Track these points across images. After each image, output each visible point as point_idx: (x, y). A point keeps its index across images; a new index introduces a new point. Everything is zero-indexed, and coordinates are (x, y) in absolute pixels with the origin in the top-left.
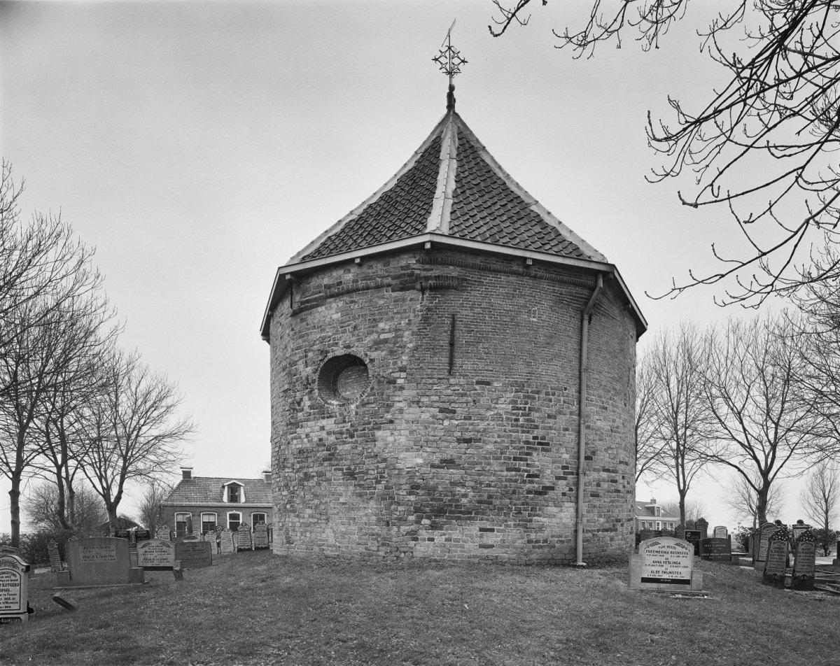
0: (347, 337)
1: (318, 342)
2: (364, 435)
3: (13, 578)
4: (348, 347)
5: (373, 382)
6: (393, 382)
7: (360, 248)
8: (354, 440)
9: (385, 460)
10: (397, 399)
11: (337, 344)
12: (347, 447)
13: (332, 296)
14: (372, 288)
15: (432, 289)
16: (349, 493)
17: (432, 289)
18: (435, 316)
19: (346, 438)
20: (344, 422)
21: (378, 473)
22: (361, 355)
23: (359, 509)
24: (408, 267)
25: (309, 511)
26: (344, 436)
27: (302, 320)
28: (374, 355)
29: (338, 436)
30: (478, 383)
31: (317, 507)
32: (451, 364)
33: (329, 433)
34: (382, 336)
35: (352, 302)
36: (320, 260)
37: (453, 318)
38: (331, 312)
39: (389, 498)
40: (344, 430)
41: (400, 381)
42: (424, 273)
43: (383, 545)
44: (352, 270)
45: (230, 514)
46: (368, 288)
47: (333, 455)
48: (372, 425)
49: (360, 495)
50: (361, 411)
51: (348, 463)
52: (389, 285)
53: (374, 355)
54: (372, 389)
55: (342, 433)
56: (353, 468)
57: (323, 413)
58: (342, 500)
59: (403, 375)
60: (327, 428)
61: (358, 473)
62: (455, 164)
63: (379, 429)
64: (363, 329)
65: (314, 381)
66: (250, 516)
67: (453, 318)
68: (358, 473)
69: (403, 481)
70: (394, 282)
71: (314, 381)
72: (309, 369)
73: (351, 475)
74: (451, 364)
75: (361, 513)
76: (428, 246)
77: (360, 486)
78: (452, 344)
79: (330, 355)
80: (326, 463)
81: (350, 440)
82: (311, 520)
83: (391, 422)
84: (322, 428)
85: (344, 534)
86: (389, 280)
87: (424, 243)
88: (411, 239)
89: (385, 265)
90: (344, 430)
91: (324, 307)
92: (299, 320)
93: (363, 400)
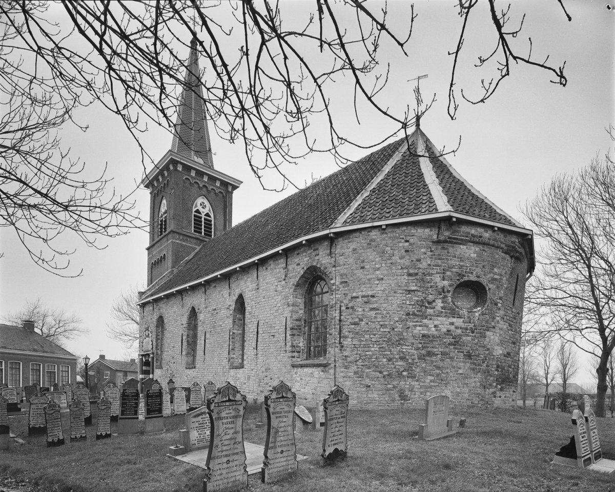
2: (480, 333)
4: (478, 277)
5: (488, 302)
6: (496, 304)
7: (387, 218)
8: (474, 335)
9: (488, 349)
10: (497, 315)
12: (469, 338)
13: (473, 242)
16: (466, 368)
19: (469, 333)
20: (470, 322)
22: (485, 284)
23: (471, 378)
24: (514, 242)
25: (430, 378)
26: (468, 331)
27: (443, 248)
28: (491, 286)
29: (464, 331)
31: (438, 375)
33: (457, 328)
35: (484, 250)
36: (420, 216)
39: (487, 372)
40: (469, 327)
43: (481, 400)
44: (489, 232)
46: (493, 246)
47: (457, 342)
49: (473, 369)
50: (481, 317)
51: (468, 348)
52: (502, 248)
53: (491, 286)
54: (488, 306)
55: (467, 329)
56: (471, 352)
57: (453, 312)
58: (460, 371)
60: (456, 324)
61: (473, 356)
63: (488, 330)
64: (487, 270)
65: (448, 292)
68: (473, 356)
69: (494, 363)
70: (505, 248)
71: (448, 292)
72: (446, 283)
73: (469, 356)
75: (472, 380)
77: (474, 364)
79: (466, 278)
80: (452, 347)
81: (471, 334)
82: (432, 384)
84: (452, 324)
85: (458, 394)
86: (503, 246)
88: (363, 224)
89: (505, 236)
90: (469, 327)
91: (465, 247)
92: (440, 247)
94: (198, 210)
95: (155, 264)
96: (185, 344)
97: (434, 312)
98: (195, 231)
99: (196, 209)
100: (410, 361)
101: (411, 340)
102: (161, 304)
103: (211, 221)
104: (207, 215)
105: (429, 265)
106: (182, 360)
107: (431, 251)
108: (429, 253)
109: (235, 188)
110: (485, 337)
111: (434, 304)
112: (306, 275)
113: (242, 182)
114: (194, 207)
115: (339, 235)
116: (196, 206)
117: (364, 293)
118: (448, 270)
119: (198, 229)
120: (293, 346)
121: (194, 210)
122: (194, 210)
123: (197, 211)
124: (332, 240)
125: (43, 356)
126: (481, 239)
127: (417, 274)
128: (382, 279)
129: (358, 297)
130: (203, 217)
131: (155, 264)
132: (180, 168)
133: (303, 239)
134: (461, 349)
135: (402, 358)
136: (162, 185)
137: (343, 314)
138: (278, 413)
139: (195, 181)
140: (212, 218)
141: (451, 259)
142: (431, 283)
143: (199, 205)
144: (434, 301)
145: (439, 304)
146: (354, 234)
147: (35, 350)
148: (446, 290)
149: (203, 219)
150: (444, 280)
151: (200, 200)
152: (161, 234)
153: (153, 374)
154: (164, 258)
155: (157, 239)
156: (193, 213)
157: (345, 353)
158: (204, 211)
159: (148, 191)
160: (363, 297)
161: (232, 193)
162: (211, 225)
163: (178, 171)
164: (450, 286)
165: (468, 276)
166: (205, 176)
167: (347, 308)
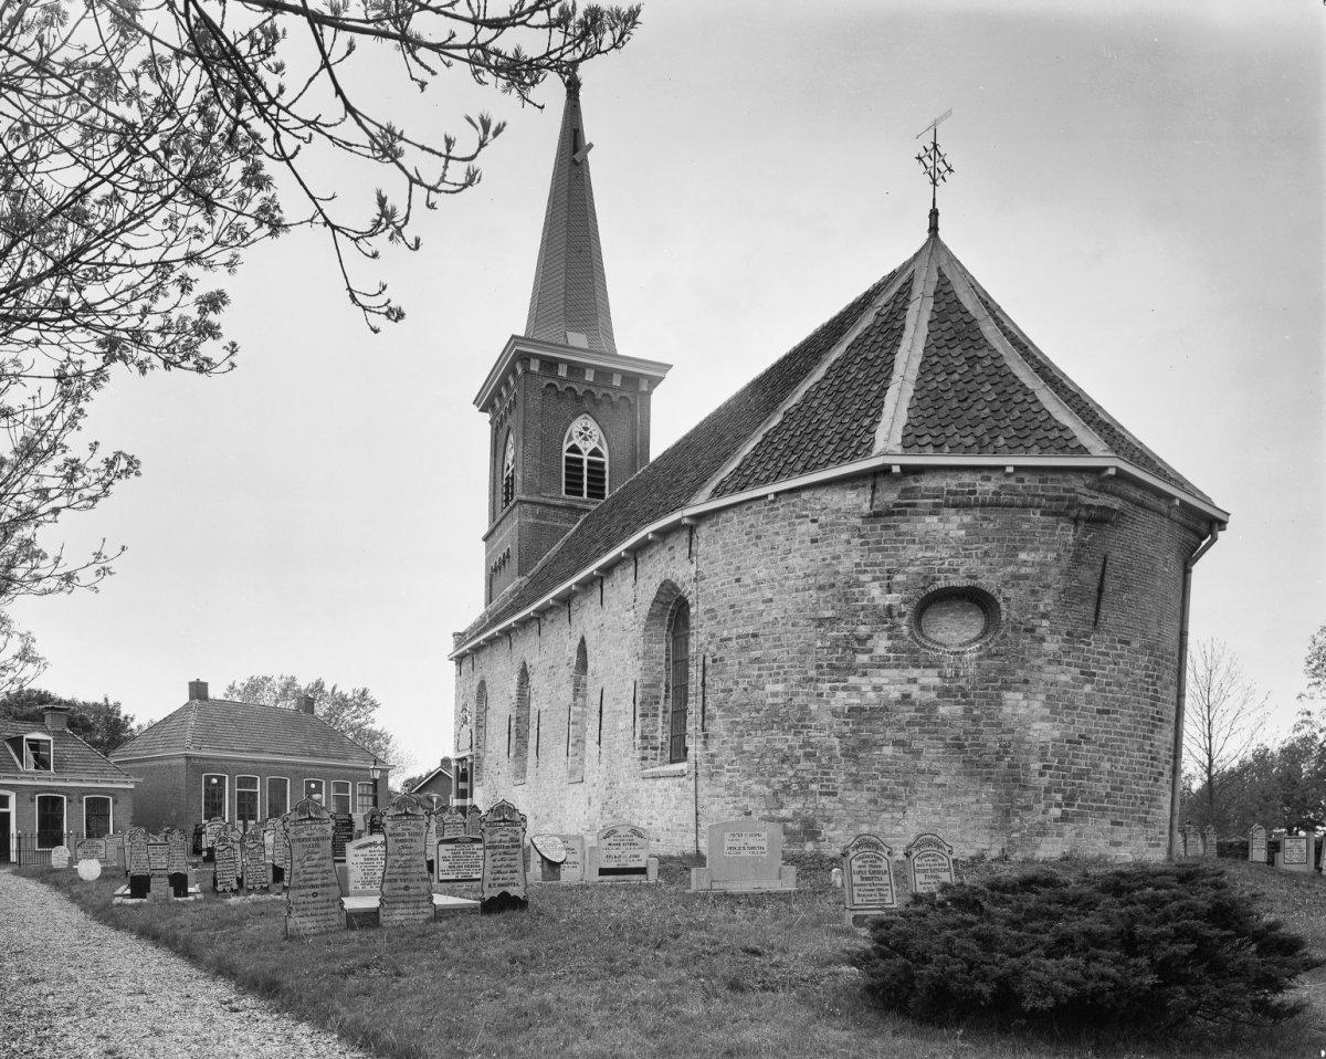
0: (973, 564)
1: (918, 563)
3: (940, 861)
4: (975, 577)
11: (955, 571)
13: (954, 506)
14: (1017, 506)
15: (1089, 520)
16: (953, 772)
17: (1089, 520)
18: (1088, 555)
21: (1000, 746)
22: (992, 590)
28: (1010, 593)
30: (1120, 642)
32: (1097, 615)
33: (923, 688)
34: (1023, 571)
35: (985, 519)
37: (1105, 559)
38: (948, 526)
41: (1040, 631)
42: (1089, 501)
45: (39, 798)
48: (999, 684)
53: (1010, 593)
58: (938, 780)
59: (1045, 623)
60: (923, 681)
62: (930, 304)
63: (1009, 689)
65: (902, 615)
66: (33, 800)
67: (1105, 559)
71: (902, 615)
74: (1097, 615)
76: (1112, 472)
78: (1100, 590)
79: (941, 584)
83: (1026, 682)
87: (1106, 468)
93: (990, 649)
94: (574, 445)
95: (495, 570)
96: (513, 735)
97: (871, 659)
98: (567, 492)
99: (571, 444)
100: (824, 761)
101: (826, 719)
102: (483, 657)
103: (602, 464)
104: (595, 452)
105: (858, 565)
106: (507, 767)
107: (861, 537)
108: (856, 541)
109: (655, 381)
110: (1001, 704)
111: (869, 644)
112: (662, 598)
113: (280, 85)
114: (565, 441)
115: (700, 518)
116: (570, 438)
117: (740, 630)
118: (898, 572)
119: (574, 487)
120: (644, 738)
121: (566, 446)
122: (566, 446)
123: (574, 449)
124: (691, 527)
125: (326, 766)
126: (973, 497)
127: (833, 586)
128: (771, 600)
129: (730, 639)
130: (586, 457)
131: (495, 570)
132: (535, 367)
133: (647, 531)
134: (936, 732)
135: (808, 756)
136: (507, 405)
137: (709, 672)
138: (399, 835)
139: (567, 385)
140: (606, 460)
141: (904, 548)
142: (863, 600)
143: (574, 435)
144: (870, 637)
145: (881, 645)
146: (724, 515)
147: (313, 755)
148: (895, 613)
149: (585, 464)
150: (890, 592)
151: (576, 426)
152: (507, 504)
153: (471, 796)
154: (508, 557)
155: (500, 516)
156: (565, 454)
157: (713, 750)
158: (586, 447)
159: (487, 417)
160: (739, 637)
161: (649, 393)
162: (603, 473)
163: (533, 373)
164: (905, 602)
165: (946, 578)
166: (588, 370)
167: (714, 661)
